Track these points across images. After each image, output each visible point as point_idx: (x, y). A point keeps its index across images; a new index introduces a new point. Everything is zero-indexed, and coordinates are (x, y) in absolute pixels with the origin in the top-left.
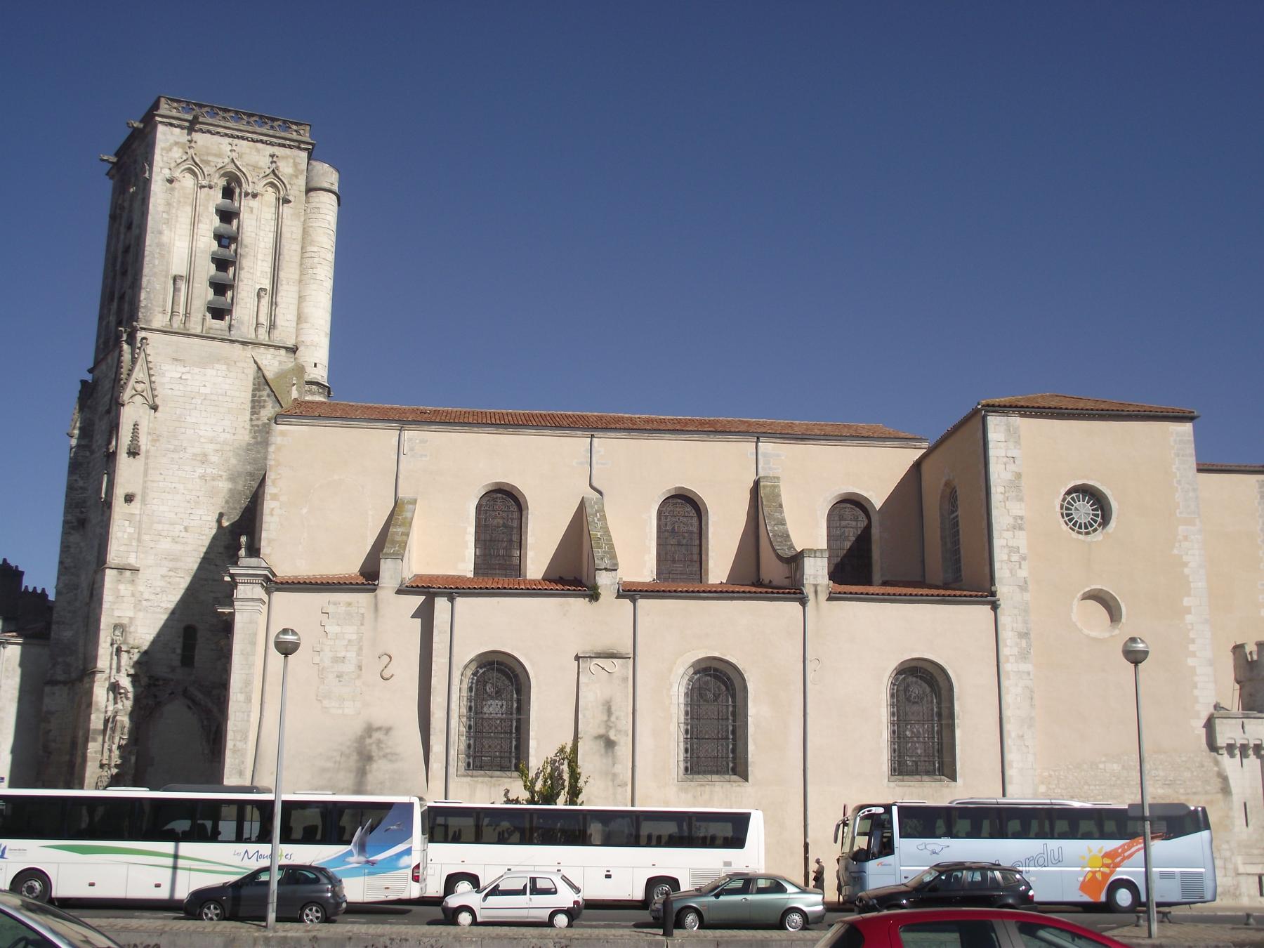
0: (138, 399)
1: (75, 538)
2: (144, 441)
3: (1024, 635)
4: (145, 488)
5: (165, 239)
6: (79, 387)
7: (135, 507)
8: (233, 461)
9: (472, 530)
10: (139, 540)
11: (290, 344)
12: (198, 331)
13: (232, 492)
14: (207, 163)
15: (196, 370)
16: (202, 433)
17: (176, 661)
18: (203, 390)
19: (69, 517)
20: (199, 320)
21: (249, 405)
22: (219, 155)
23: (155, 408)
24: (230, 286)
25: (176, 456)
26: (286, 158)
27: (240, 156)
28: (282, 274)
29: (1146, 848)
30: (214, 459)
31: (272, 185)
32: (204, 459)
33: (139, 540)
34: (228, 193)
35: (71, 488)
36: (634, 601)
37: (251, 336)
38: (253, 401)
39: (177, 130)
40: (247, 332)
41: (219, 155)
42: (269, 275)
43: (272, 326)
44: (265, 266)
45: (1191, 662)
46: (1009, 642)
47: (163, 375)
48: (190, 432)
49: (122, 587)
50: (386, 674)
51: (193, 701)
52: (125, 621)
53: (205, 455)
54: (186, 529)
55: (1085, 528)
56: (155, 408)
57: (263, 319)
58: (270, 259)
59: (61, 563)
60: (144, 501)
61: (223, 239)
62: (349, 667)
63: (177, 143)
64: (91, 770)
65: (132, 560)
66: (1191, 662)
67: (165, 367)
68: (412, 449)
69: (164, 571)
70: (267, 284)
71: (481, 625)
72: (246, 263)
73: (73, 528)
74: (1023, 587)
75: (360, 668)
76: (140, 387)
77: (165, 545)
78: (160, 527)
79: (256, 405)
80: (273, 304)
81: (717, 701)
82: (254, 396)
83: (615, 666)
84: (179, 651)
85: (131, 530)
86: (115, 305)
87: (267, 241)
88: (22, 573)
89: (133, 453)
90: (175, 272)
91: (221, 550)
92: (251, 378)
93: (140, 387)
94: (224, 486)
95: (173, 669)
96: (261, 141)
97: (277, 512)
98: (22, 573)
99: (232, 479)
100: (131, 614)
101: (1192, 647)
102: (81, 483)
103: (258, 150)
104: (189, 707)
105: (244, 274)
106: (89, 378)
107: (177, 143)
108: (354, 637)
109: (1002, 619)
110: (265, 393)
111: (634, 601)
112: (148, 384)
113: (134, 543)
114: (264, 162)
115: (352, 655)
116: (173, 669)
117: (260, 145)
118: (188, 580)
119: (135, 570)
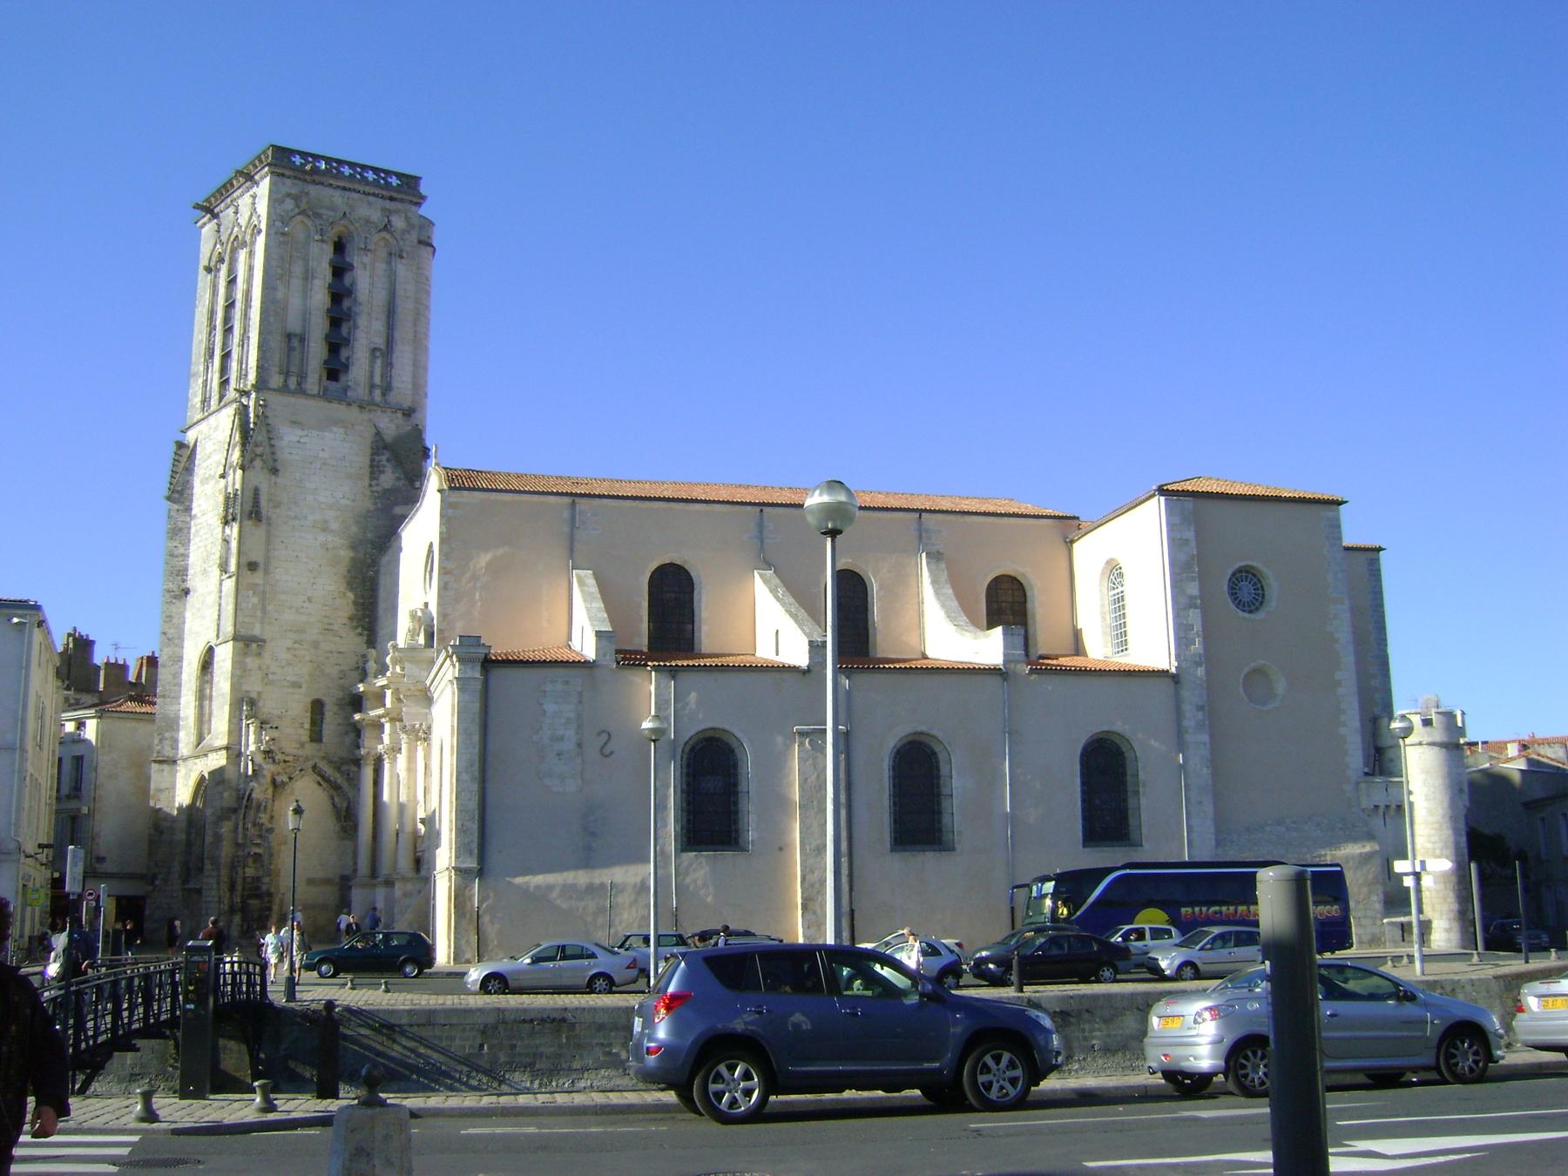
4: (267, 558)
8: (354, 529)
9: (646, 604)
10: (264, 611)
11: (407, 404)
13: (353, 560)
15: (315, 433)
16: (321, 499)
17: (306, 738)
18: (321, 454)
19: (171, 586)
20: (312, 384)
21: (367, 470)
22: (333, 208)
23: (274, 471)
24: (347, 342)
25: (297, 523)
26: (397, 212)
28: (397, 334)
30: (334, 526)
33: (264, 611)
34: (339, 247)
38: (372, 466)
39: (288, 182)
44: (379, 326)
45: (1342, 731)
46: (1188, 715)
47: (281, 438)
48: (310, 498)
49: (249, 660)
50: (607, 751)
51: (323, 777)
52: (254, 695)
53: (326, 522)
55: (1239, 603)
56: (274, 471)
57: (377, 380)
58: (383, 317)
60: (266, 572)
62: (569, 746)
63: (289, 195)
64: (1320, 908)
66: (1342, 731)
69: (289, 643)
70: (380, 342)
72: (362, 321)
73: (175, 597)
75: (579, 745)
76: (259, 450)
77: (289, 616)
78: (283, 597)
79: (375, 470)
80: (388, 365)
82: (372, 460)
84: (307, 726)
85: (255, 600)
87: (381, 297)
88: (93, 642)
91: (346, 621)
92: (369, 442)
93: (259, 450)
94: (346, 554)
95: (302, 745)
96: (374, 195)
98: (93, 642)
99: (353, 547)
100: (259, 688)
101: (1343, 718)
103: (370, 204)
107: (289, 195)
108: (572, 715)
110: (384, 458)
113: (259, 614)
115: (571, 733)
116: (302, 745)
117: (371, 198)
118: (1356, 698)
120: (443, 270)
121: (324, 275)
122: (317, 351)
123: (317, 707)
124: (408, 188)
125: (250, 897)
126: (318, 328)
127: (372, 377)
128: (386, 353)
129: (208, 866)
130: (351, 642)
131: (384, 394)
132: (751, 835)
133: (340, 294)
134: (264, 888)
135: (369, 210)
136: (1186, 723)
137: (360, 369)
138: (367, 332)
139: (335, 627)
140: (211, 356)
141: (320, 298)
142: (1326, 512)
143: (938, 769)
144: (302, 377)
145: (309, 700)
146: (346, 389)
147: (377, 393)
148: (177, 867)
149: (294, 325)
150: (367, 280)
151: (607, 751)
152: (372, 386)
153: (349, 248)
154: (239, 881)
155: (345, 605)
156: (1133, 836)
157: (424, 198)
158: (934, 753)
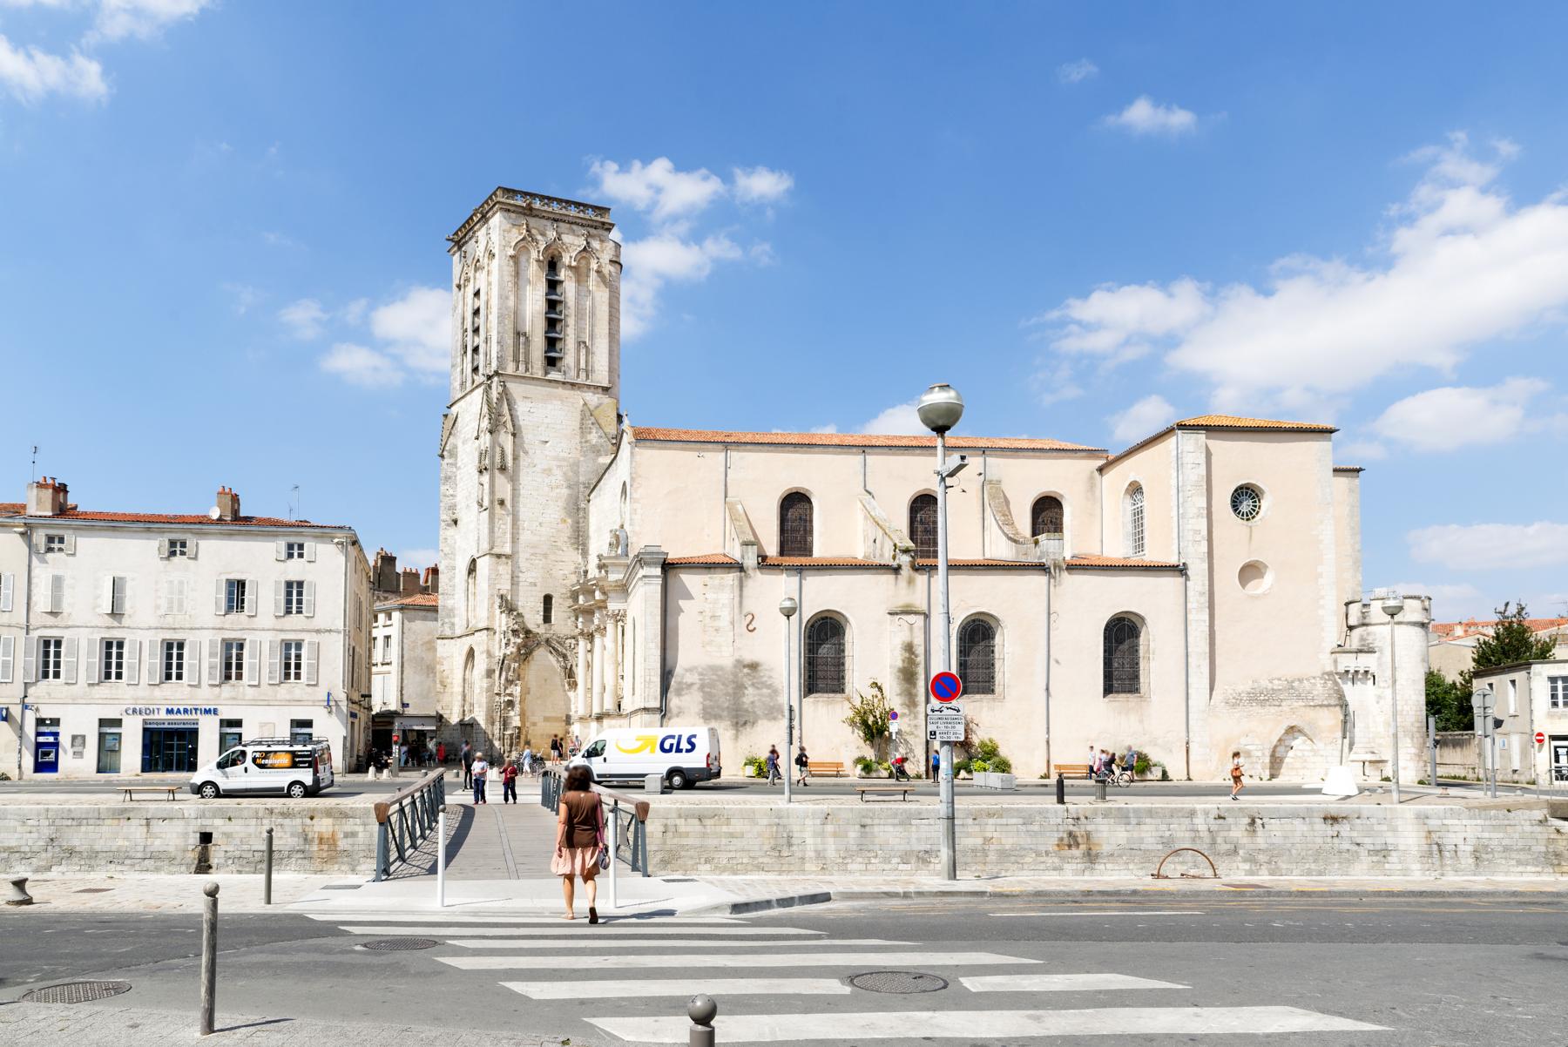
32: (548, 472)
61: (552, 305)
71: (468, 641)
79: (583, 430)
81: (824, 634)
89: (503, 469)
123: (548, 600)
137: (569, 359)
155: (566, 530)
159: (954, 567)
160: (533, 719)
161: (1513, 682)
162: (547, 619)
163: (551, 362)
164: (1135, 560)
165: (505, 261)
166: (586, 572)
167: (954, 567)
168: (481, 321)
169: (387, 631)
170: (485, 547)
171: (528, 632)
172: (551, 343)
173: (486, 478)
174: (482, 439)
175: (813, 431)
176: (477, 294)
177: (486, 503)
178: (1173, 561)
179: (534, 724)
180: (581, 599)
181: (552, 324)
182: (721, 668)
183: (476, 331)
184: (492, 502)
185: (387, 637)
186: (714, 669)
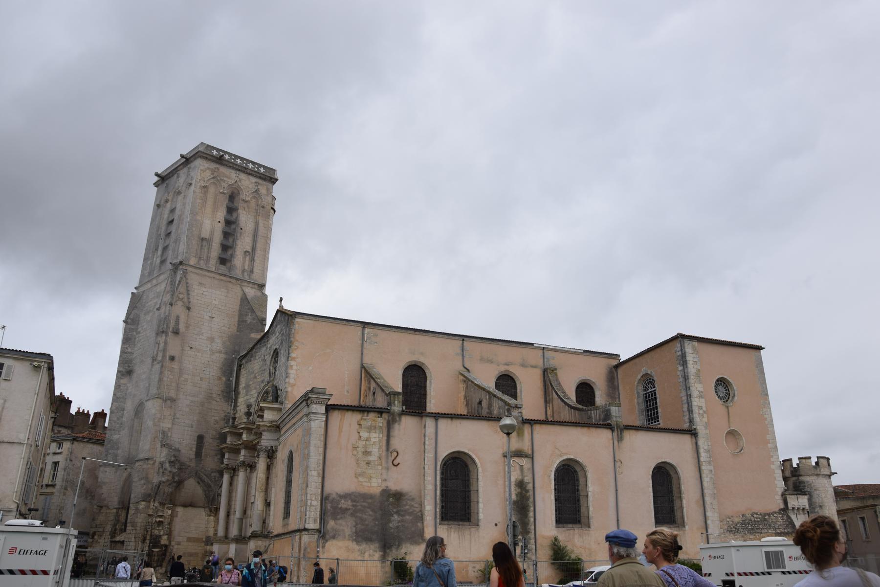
0: (180, 303)
1: (124, 381)
2: (182, 327)
3: (708, 451)
5: (199, 218)
6: (130, 296)
7: (175, 365)
12: (213, 270)
14: (224, 181)
23: (189, 309)
27: (240, 181)
29: (300, 539)
31: (254, 197)
35: (123, 352)
36: (436, 420)
37: (240, 277)
40: (238, 273)
41: (229, 178)
42: (251, 245)
43: (252, 271)
45: (773, 467)
50: (396, 463)
54: (201, 379)
56: (189, 309)
58: (251, 236)
59: (114, 395)
61: (228, 223)
65: (172, 394)
66: (773, 467)
67: (195, 287)
68: (369, 338)
70: (249, 248)
73: (123, 375)
74: (706, 428)
80: (253, 260)
81: (457, 472)
83: (524, 462)
86: (159, 253)
88: (71, 402)
89: (176, 332)
90: (203, 235)
93: (181, 296)
95: (191, 460)
97: (294, 368)
98: (71, 402)
102: (129, 350)
104: (199, 483)
105: (239, 242)
106: (135, 291)
108: (377, 440)
109: (700, 443)
111: (436, 420)
112: (185, 296)
114: (253, 188)
119: (173, 400)
120: (278, 223)
121: (221, 214)
122: (215, 250)
123: (200, 439)
124: (269, 177)
125: (154, 547)
126: (218, 238)
127: (244, 266)
128: (251, 254)
129: (129, 528)
130: (220, 408)
131: (249, 276)
132: (481, 516)
133: (230, 227)
134: (163, 543)
135: (247, 183)
136: (702, 459)
137: (239, 261)
138: (243, 243)
139: (214, 396)
140: (157, 250)
141: (219, 228)
142: (753, 352)
143: (578, 480)
144: (207, 261)
145: (197, 434)
146: (230, 270)
147: (246, 274)
148: (109, 528)
149: (205, 234)
150: (245, 219)
151: (396, 463)
152: (244, 271)
153: (236, 200)
154: (148, 537)
156: (679, 520)
157: (277, 180)
158: (575, 471)
159: (437, 416)
160: (178, 539)
161: (863, 519)
162: (198, 454)
163: (223, 261)
164: (286, 531)
165: (198, 190)
166: (234, 419)
167: (437, 416)
168: (173, 228)
169: (57, 458)
170: (153, 391)
171: (182, 464)
172: (225, 248)
173: (161, 339)
174: (162, 310)
175: (763, 539)
176: (173, 211)
177: (160, 358)
178: (686, 426)
179: (179, 543)
180: (229, 440)
181: (226, 235)
182: (371, 497)
183: (169, 234)
184: (164, 356)
185: (56, 464)
186: (365, 497)
